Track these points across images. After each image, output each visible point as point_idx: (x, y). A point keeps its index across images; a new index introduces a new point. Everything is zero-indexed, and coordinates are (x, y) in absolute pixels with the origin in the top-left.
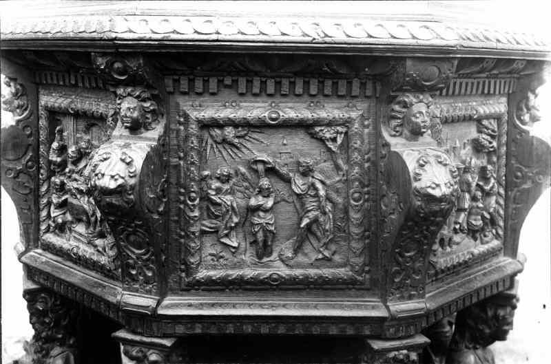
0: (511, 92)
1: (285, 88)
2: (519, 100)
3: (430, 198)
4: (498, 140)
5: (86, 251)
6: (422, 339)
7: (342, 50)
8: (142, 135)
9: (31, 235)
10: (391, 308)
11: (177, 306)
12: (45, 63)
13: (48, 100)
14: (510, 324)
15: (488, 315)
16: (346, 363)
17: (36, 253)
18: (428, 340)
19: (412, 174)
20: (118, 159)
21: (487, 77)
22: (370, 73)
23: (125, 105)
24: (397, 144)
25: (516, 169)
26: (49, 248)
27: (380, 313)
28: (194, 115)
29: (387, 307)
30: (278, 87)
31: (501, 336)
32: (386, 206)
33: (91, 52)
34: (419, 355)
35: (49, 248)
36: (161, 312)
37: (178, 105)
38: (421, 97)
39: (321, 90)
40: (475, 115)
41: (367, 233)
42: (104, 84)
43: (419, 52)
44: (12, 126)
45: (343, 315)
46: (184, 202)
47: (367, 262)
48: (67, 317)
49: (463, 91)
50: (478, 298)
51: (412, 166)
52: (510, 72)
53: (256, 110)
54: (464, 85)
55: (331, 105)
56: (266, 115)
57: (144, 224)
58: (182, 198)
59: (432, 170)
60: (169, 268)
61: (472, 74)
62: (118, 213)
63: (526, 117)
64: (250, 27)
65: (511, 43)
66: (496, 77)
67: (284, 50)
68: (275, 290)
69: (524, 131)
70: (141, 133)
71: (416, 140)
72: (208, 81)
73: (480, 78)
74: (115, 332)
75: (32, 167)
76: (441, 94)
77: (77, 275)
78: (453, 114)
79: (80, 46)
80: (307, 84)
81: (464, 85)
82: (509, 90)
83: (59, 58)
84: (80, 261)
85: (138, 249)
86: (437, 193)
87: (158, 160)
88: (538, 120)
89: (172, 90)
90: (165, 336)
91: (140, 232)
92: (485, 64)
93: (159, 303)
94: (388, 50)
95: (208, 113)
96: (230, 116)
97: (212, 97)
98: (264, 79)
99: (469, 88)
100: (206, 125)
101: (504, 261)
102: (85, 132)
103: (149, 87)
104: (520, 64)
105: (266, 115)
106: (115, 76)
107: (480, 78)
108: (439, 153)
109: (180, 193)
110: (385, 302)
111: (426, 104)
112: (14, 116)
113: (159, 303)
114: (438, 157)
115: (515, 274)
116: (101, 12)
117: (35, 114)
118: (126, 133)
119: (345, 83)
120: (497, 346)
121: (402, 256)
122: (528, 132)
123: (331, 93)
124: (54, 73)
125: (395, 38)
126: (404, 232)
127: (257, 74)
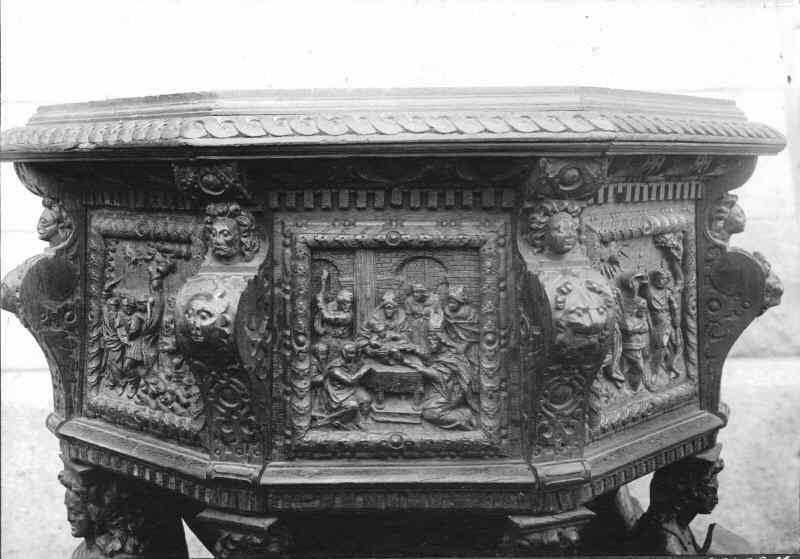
0: (699, 196)
1: (327, 202)
3: (578, 329)
4: (270, 239)
7: (401, 151)
9: (71, 395)
10: (540, 473)
11: (279, 474)
12: (73, 177)
13: (101, 222)
17: (116, 418)
19: (551, 298)
20: (215, 294)
22: (495, 179)
23: (219, 227)
25: (735, 292)
26: (98, 413)
29: (534, 470)
30: (478, 199)
34: (580, 533)
36: (265, 480)
42: (195, 204)
43: (338, 152)
45: (441, 480)
46: (291, 348)
48: (105, 495)
49: (662, 196)
51: (550, 291)
52: (706, 169)
53: (369, 228)
57: (228, 372)
59: (579, 291)
60: (267, 430)
64: (524, 122)
65: (740, 135)
66: (679, 178)
67: (408, 152)
68: (396, 457)
70: (235, 263)
71: (559, 259)
76: (596, 200)
77: (138, 447)
78: (622, 229)
79: (492, 150)
80: (318, 197)
82: (696, 195)
85: (229, 403)
86: (586, 321)
87: (257, 299)
93: (261, 473)
94: (381, 151)
96: (378, 237)
97: (431, 213)
99: (686, 192)
101: (700, 414)
109: (285, 336)
110: (528, 461)
113: (261, 473)
115: (716, 430)
122: (725, 248)
126: (556, 368)
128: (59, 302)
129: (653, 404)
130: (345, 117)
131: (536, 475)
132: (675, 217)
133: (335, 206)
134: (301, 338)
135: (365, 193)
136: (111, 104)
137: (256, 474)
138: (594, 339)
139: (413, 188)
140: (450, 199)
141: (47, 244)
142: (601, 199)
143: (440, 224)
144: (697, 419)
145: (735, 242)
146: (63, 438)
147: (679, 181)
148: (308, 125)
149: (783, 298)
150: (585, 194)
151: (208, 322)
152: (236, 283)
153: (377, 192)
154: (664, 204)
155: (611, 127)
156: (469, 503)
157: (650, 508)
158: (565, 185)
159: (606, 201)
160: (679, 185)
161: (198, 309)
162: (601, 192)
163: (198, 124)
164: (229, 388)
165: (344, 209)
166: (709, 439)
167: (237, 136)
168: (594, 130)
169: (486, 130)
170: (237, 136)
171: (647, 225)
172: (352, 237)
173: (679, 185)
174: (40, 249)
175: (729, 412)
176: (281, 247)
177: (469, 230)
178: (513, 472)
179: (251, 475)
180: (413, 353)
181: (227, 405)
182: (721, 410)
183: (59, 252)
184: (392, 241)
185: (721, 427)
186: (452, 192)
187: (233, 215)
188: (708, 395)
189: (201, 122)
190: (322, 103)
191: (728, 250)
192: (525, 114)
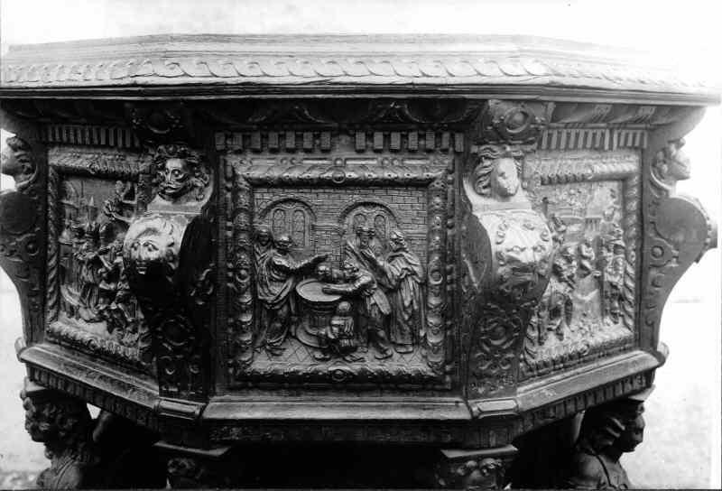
8: (183, 205)
9: (35, 326)
12: (45, 115)
13: (60, 158)
15: (613, 417)
17: (74, 345)
18: (516, 449)
20: (157, 232)
22: (450, 121)
25: (660, 236)
27: (462, 414)
28: (241, 171)
36: (208, 415)
38: (508, 149)
40: (590, 176)
44: (14, 193)
47: (449, 357)
48: (53, 410)
50: (614, 395)
52: (650, 123)
54: (573, 138)
57: (185, 310)
58: (230, 274)
59: (513, 229)
61: (626, 123)
64: (437, 66)
69: (660, 189)
73: (599, 128)
75: (31, 238)
76: (540, 144)
81: (573, 138)
84: (99, 355)
88: (683, 178)
89: (259, 147)
91: (504, 343)
95: (257, 174)
100: (258, 184)
102: (598, 238)
106: (156, 131)
107: (599, 128)
113: (202, 410)
117: (42, 177)
120: (625, 458)
121: (488, 344)
122: (670, 193)
124: (112, 131)
125: (428, 76)
126: (495, 312)
129: (588, 346)
131: (471, 412)
134: (243, 272)
136: (490, 40)
137: (198, 412)
138: (528, 277)
140: (396, 141)
144: (639, 358)
145: (679, 190)
146: (32, 368)
147: (625, 128)
148: (411, 68)
151: (153, 255)
152: (180, 220)
153: (305, 134)
154: (554, 154)
155: (542, 71)
156: (382, 438)
158: (512, 129)
166: (648, 375)
167: (183, 75)
168: (556, 75)
169: (346, 75)
170: (183, 75)
171: (589, 171)
173: (624, 133)
175: (668, 353)
177: (413, 168)
178: (451, 410)
181: (174, 344)
182: (660, 348)
183: (22, 189)
184: (339, 179)
185: (658, 366)
186: (399, 135)
188: (645, 335)
190: (480, 47)
191: (672, 195)
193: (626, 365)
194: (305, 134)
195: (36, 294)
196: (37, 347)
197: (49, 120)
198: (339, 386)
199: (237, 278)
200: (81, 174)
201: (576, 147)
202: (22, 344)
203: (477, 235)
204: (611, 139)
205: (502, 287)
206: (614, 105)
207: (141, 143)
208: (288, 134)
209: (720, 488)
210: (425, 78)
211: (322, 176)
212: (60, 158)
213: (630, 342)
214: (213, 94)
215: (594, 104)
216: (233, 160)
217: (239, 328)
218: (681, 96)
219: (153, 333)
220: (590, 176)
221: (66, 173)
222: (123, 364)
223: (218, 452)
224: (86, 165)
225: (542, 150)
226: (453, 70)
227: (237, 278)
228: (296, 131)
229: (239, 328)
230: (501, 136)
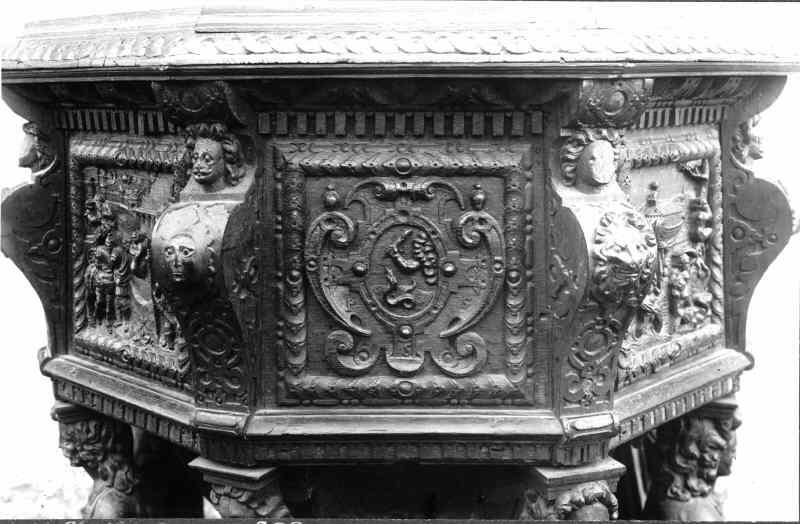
2: (735, 138)
5: (140, 352)
6: (614, 465)
9: (61, 334)
11: (269, 422)
12: (58, 100)
13: (80, 148)
14: (734, 451)
16: (430, 510)
17: (106, 356)
20: (191, 225)
21: (691, 105)
22: (527, 107)
24: (569, 197)
25: (742, 230)
26: (86, 349)
27: (553, 428)
28: (296, 161)
31: (297, 512)
32: (578, 285)
33: (150, 82)
35: (86, 349)
36: (253, 430)
37: (275, 152)
39: (449, 127)
41: (530, 319)
42: (180, 123)
44: (31, 186)
48: (93, 429)
52: (720, 95)
54: (697, 113)
55: (422, 150)
56: (393, 162)
62: (193, 295)
63: (745, 153)
72: (314, 118)
74: (191, 460)
76: (638, 128)
83: (101, 93)
84: (133, 365)
90: (257, 466)
92: (685, 85)
98: (391, 115)
100: (309, 173)
103: (233, 126)
104: (693, 82)
105: (393, 162)
107: (710, 105)
108: (631, 211)
111: (611, 142)
112: (34, 172)
114: (631, 215)
116: (92, 21)
118: (200, 190)
119: (442, 118)
123: (521, 133)
127: (383, 109)
128: (53, 236)
130: (303, 29)
132: (704, 142)
133: (409, 131)
135: (324, 116)
139: (535, 110)
141: (29, 170)
142: (642, 125)
143: (449, 153)
145: (759, 169)
146: (57, 381)
149: (18, 163)
150: (626, 121)
157: (623, 463)
158: (610, 111)
159: (662, 125)
160: (698, 109)
161: (621, 309)
162: (643, 118)
163: (206, 43)
164: (216, 333)
165: (340, 137)
167: (272, 52)
169: (430, 51)
172: (317, 162)
174: (27, 177)
176: (272, 181)
178: (540, 422)
179: (237, 424)
180: (692, 331)
187: (218, 138)
188: (735, 335)
189: (209, 39)
192: (288, 35)
193: (699, 374)
194: (397, 116)
195: (56, 300)
196: (61, 359)
197: (71, 105)
198: (407, 401)
199: (288, 280)
200: (104, 164)
201: (700, 122)
202: (48, 353)
203: (567, 225)
204: (84, 118)
205: (602, 287)
206: (744, 77)
207: (175, 129)
208: (318, 115)
209: (797, 520)
210: (485, 56)
211: (343, 165)
212: (80, 148)
213: (174, 378)
214: (249, 74)
215: (726, 78)
216: (285, 147)
217: (292, 330)
218: (777, 69)
219: (190, 341)
220: (675, 157)
221: (84, 163)
222: (157, 376)
223: (257, 474)
224: (113, 153)
225: (79, 131)
226: (223, 39)
227: (288, 280)
228: (465, 112)
229: (292, 330)
230: (597, 120)
